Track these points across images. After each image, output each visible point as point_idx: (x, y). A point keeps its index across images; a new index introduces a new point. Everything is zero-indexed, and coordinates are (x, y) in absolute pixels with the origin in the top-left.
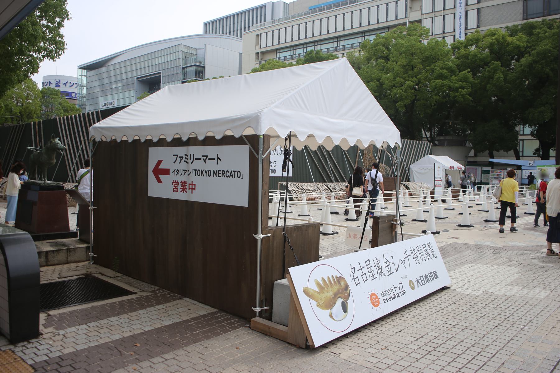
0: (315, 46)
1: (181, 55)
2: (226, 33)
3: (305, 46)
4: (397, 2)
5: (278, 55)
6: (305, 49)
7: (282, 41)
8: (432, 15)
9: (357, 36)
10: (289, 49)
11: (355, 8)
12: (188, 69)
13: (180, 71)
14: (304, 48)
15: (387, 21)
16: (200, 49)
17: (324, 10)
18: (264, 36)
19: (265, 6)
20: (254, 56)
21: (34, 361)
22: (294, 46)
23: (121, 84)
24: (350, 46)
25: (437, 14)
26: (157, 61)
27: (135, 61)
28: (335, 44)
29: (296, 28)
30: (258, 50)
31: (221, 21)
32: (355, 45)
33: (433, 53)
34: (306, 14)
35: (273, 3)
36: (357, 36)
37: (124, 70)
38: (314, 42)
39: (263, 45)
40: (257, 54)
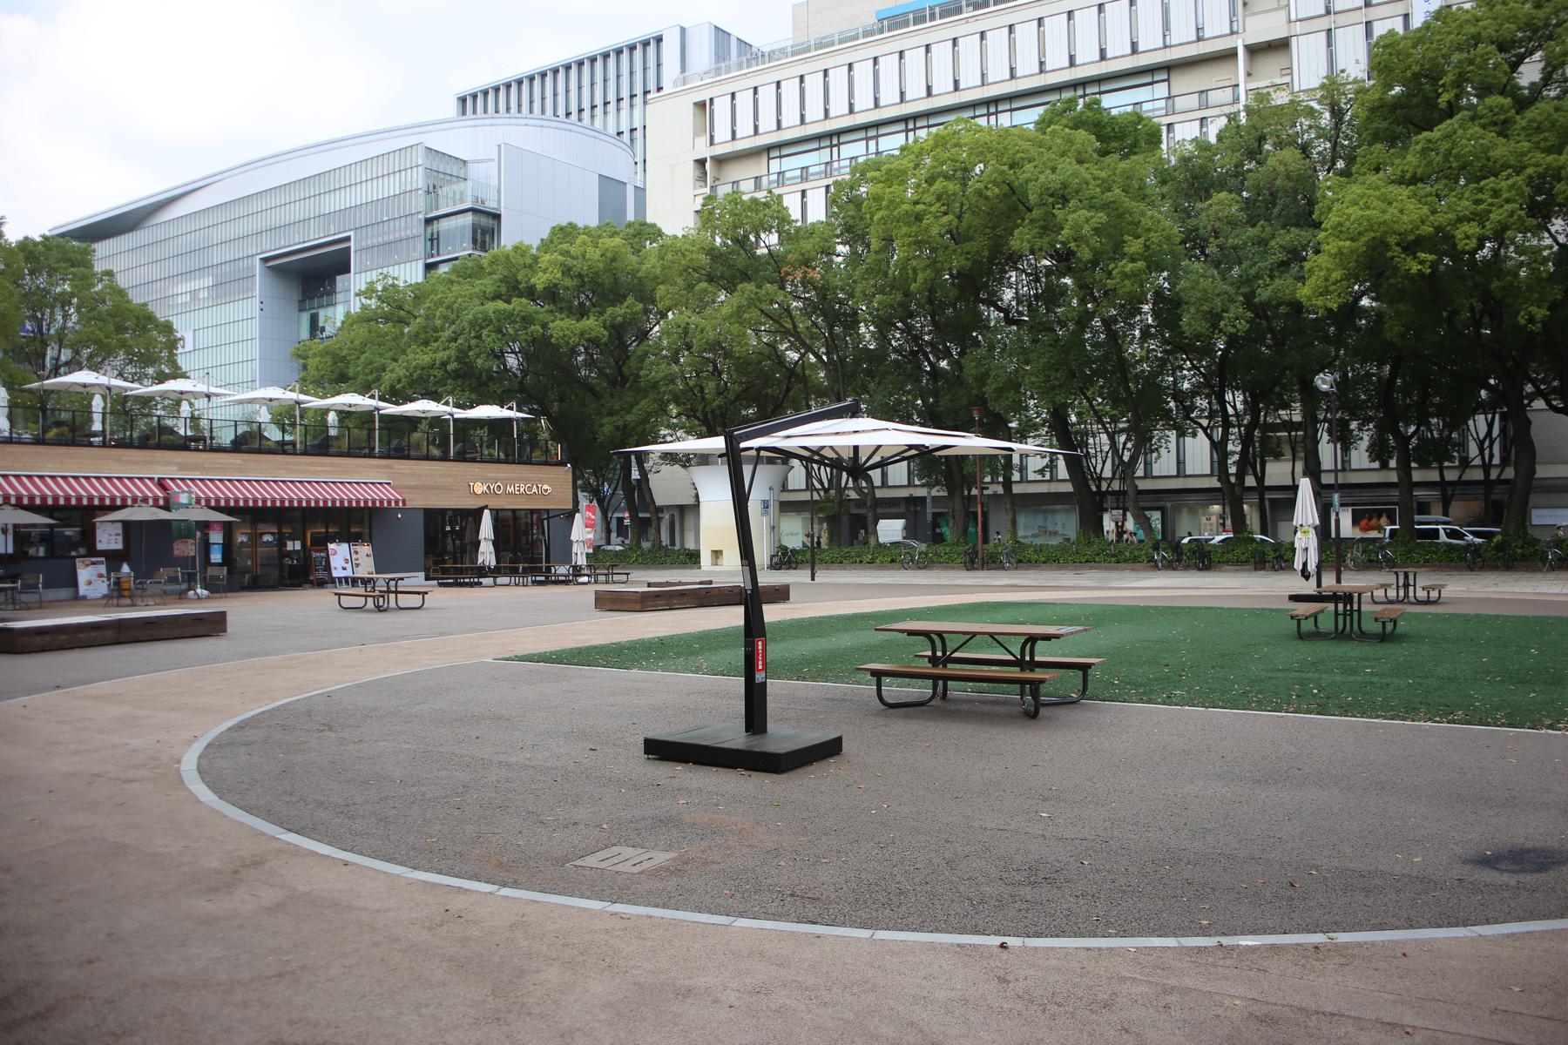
0: (907, 131)
1: (418, 179)
2: (568, 114)
3: (872, 133)
4: (1101, 7)
5: (775, 165)
6: (872, 143)
7: (745, 128)
8: (1325, 23)
9: (1149, 79)
10: (815, 145)
11: (993, 19)
12: (444, 225)
13: (418, 229)
14: (867, 139)
15: (1199, 39)
16: (478, 162)
18: (722, 109)
19: (659, 40)
20: (690, 170)
22: (829, 135)
23: (209, 281)
24: (798, 173)
25: (1341, 20)
26: (333, 203)
28: (824, 155)
29: (745, 101)
30: (706, 152)
31: (514, 89)
32: (811, 170)
34: (867, 34)
37: (218, 235)
38: (904, 119)
39: (722, 132)
40: (701, 163)
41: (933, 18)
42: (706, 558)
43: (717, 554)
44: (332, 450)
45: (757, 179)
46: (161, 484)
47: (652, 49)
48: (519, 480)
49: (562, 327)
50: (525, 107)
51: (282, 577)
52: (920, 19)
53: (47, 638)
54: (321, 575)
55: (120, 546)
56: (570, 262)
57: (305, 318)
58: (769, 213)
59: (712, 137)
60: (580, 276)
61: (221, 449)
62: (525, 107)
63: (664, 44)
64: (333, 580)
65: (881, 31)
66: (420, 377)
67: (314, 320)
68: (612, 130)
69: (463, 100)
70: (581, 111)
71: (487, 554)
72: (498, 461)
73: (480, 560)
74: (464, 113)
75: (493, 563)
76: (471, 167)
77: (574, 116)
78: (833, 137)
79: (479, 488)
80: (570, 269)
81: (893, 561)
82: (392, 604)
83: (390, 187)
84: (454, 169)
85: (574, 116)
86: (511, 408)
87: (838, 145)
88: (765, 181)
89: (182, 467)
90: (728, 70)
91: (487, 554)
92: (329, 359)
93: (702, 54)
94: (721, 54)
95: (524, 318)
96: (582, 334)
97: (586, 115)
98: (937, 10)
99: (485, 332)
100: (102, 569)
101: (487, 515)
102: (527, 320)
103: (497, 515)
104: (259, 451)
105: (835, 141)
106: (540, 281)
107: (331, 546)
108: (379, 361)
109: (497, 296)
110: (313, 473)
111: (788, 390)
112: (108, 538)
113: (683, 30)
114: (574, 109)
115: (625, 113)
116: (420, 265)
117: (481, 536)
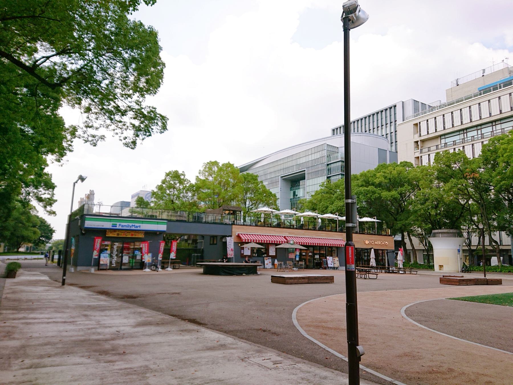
1: (325, 153)
2: (366, 131)
5: (443, 141)
6: (479, 131)
12: (332, 165)
13: (325, 167)
14: (477, 130)
15: (480, 119)
17: (500, 88)
19: (395, 106)
20: (413, 145)
21: (78, 180)
27: (279, 163)
28: (462, 136)
31: (367, 119)
32: (457, 141)
33: (395, 172)
35: (403, 102)
36: (499, 122)
39: (424, 132)
40: (417, 142)
41: (500, 88)
42: (436, 267)
43: (441, 266)
44: (304, 228)
45: (437, 146)
46: (285, 237)
47: (393, 109)
48: (378, 240)
49: (385, 194)
50: (356, 130)
51: (314, 266)
52: (495, 88)
53: (292, 281)
54: (325, 266)
55: (275, 254)
56: (386, 175)
57: (292, 192)
58: (460, 156)
59: (420, 134)
60: (390, 179)
61: (274, 227)
62: (356, 130)
63: (397, 107)
64: (328, 268)
65: (480, 94)
66: (340, 209)
67: (294, 193)
68: (380, 134)
69: (334, 130)
70: (370, 130)
71: (373, 263)
72: (372, 234)
73: (371, 264)
74: (334, 134)
75: (375, 265)
76: (339, 149)
77: (368, 132)
78: (465, 130)
79: (367, 242)
80: (386, 177)
81: (509, 272)
82: (368, 277)
83: (317, 156)
84: (335, 150)
85: (368, 132)
86: (374, 219)
87: (466, 133)
88: (440, 146)
89: (289, 233)
90: (425, 113)
91: (373, 263)
92: (311, 204)
93: (410, 110)
94: (416, 109)
95: (373, 192)
96: (391, 197)
97: (371, 131)
98: (502, 85)
99: (360, 196)
100: (270, 260)
101: (373, 250)
102: (374, 193)
103: (376, 251)
104: (284, 228)
105: (465, 132)
106: (377, 181)
107: (328, 257)
108: (326, 205)
109: (362, 186)
110: (322, 236)
111: (462, 213)
112: (272, 252)
113: (403, 102)
114: (367, 129)
115: (388, 129)
116: (326, 177)
117: (371, 257)
